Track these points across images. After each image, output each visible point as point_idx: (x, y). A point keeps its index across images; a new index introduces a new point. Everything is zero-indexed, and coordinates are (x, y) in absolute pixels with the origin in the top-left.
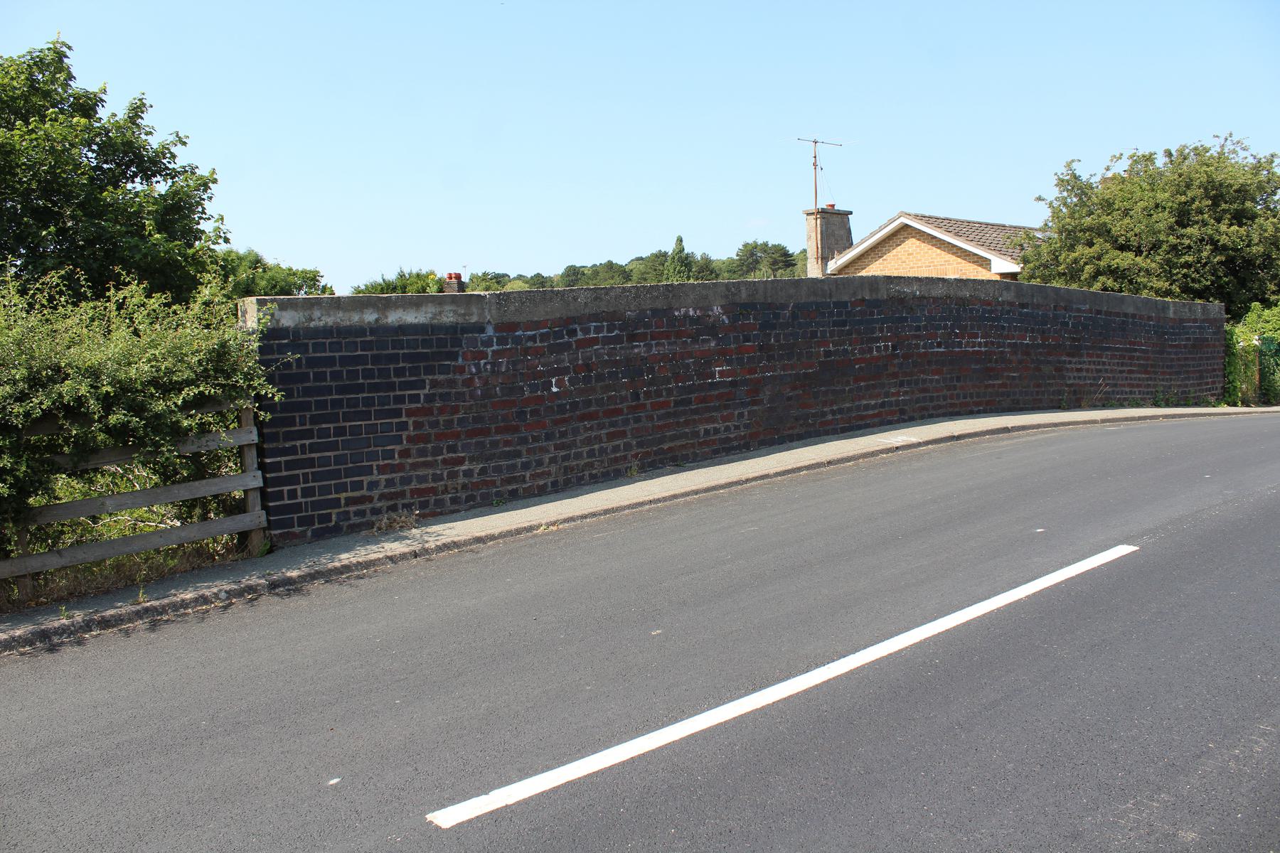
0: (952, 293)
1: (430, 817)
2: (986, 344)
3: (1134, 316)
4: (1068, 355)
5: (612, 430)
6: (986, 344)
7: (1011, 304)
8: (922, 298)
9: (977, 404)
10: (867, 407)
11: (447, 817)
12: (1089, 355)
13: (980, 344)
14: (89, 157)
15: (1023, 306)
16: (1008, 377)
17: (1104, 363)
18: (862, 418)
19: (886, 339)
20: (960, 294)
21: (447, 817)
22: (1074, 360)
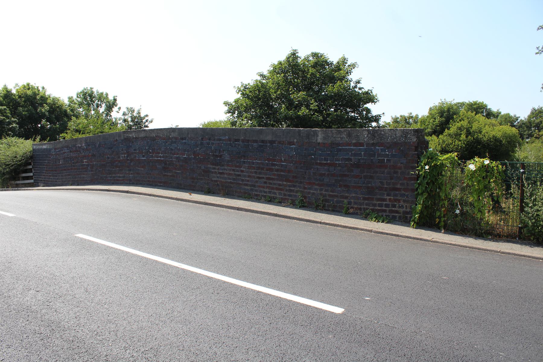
0: (148, 135)
1: (343, 310)
2: (163, 157)
3: (272, 142)
4: (213, 164)
5: (331, 193)
6: (163, 157)
7: (176, 138)
8: (136, 138)
9: (161, 182)
10: (120, 177)
11: (338, 310)
12: (228, 165)
13: (160, 157)
14: (369, 135)
15: (182, 139)
16: (176, 173)
17: (242, 171)
18: (118, 180)
19: (125, 154)
20: (151, 135)
21: (338, 310)
22: (217, 167)
